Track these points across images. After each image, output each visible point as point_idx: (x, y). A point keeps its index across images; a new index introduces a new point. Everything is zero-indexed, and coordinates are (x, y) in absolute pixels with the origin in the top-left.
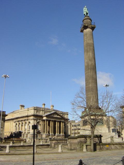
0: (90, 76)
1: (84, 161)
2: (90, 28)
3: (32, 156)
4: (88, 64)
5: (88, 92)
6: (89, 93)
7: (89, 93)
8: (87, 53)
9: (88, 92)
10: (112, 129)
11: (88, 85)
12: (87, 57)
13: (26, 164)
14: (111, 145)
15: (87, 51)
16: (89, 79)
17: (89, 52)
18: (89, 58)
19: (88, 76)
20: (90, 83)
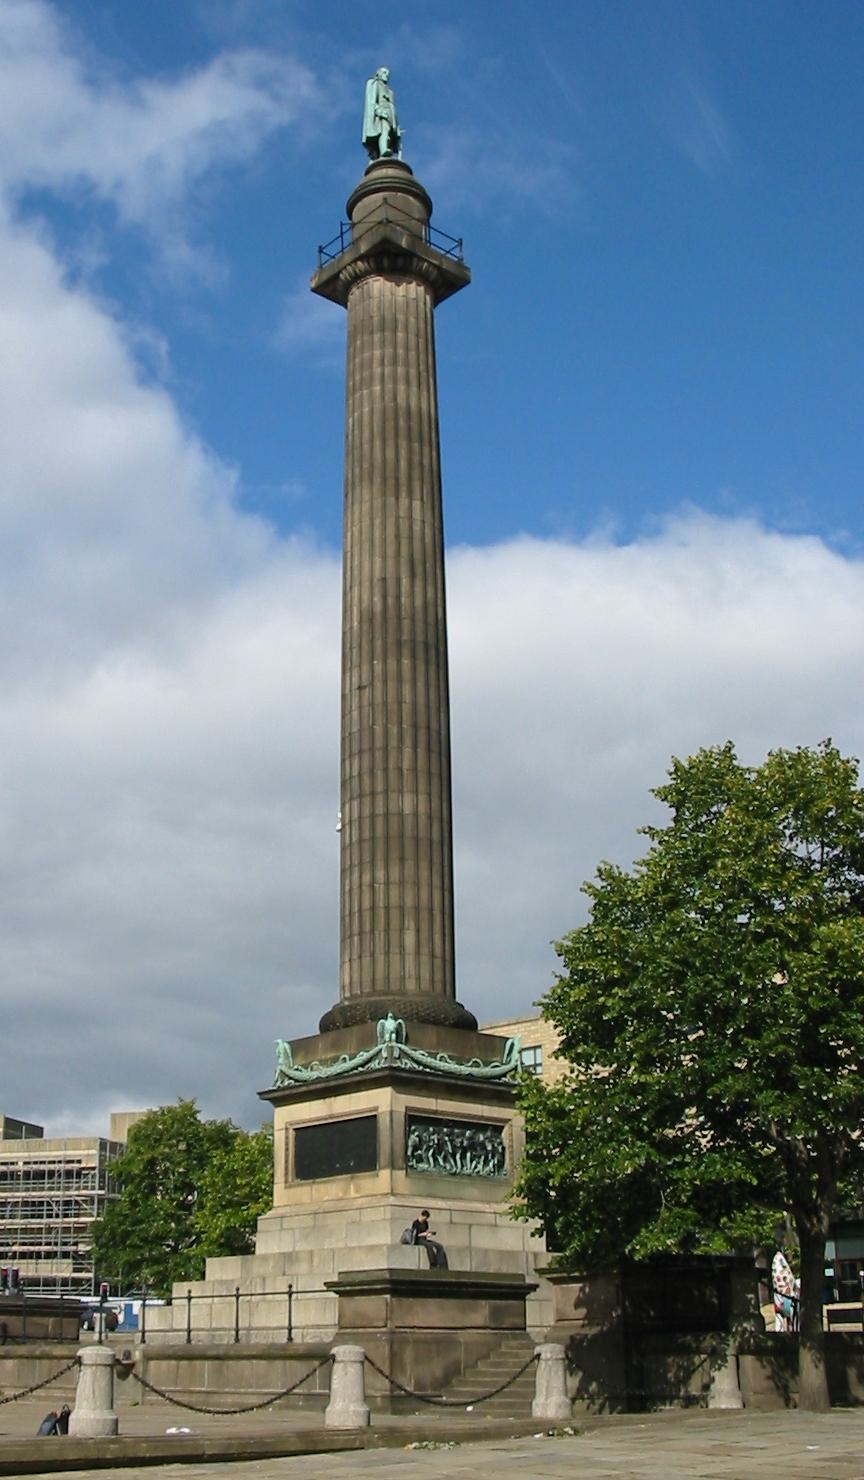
0: (406, 709)
4: (390, 601)
5: (380, 864)
7: (395, 875)
8: (391, 500)
9: (380, 864)
12: (391, 530)
14: (357, 278)
15: (391, 482)
16: (393, 742)
17: (403, 494)
18: (404, 542)
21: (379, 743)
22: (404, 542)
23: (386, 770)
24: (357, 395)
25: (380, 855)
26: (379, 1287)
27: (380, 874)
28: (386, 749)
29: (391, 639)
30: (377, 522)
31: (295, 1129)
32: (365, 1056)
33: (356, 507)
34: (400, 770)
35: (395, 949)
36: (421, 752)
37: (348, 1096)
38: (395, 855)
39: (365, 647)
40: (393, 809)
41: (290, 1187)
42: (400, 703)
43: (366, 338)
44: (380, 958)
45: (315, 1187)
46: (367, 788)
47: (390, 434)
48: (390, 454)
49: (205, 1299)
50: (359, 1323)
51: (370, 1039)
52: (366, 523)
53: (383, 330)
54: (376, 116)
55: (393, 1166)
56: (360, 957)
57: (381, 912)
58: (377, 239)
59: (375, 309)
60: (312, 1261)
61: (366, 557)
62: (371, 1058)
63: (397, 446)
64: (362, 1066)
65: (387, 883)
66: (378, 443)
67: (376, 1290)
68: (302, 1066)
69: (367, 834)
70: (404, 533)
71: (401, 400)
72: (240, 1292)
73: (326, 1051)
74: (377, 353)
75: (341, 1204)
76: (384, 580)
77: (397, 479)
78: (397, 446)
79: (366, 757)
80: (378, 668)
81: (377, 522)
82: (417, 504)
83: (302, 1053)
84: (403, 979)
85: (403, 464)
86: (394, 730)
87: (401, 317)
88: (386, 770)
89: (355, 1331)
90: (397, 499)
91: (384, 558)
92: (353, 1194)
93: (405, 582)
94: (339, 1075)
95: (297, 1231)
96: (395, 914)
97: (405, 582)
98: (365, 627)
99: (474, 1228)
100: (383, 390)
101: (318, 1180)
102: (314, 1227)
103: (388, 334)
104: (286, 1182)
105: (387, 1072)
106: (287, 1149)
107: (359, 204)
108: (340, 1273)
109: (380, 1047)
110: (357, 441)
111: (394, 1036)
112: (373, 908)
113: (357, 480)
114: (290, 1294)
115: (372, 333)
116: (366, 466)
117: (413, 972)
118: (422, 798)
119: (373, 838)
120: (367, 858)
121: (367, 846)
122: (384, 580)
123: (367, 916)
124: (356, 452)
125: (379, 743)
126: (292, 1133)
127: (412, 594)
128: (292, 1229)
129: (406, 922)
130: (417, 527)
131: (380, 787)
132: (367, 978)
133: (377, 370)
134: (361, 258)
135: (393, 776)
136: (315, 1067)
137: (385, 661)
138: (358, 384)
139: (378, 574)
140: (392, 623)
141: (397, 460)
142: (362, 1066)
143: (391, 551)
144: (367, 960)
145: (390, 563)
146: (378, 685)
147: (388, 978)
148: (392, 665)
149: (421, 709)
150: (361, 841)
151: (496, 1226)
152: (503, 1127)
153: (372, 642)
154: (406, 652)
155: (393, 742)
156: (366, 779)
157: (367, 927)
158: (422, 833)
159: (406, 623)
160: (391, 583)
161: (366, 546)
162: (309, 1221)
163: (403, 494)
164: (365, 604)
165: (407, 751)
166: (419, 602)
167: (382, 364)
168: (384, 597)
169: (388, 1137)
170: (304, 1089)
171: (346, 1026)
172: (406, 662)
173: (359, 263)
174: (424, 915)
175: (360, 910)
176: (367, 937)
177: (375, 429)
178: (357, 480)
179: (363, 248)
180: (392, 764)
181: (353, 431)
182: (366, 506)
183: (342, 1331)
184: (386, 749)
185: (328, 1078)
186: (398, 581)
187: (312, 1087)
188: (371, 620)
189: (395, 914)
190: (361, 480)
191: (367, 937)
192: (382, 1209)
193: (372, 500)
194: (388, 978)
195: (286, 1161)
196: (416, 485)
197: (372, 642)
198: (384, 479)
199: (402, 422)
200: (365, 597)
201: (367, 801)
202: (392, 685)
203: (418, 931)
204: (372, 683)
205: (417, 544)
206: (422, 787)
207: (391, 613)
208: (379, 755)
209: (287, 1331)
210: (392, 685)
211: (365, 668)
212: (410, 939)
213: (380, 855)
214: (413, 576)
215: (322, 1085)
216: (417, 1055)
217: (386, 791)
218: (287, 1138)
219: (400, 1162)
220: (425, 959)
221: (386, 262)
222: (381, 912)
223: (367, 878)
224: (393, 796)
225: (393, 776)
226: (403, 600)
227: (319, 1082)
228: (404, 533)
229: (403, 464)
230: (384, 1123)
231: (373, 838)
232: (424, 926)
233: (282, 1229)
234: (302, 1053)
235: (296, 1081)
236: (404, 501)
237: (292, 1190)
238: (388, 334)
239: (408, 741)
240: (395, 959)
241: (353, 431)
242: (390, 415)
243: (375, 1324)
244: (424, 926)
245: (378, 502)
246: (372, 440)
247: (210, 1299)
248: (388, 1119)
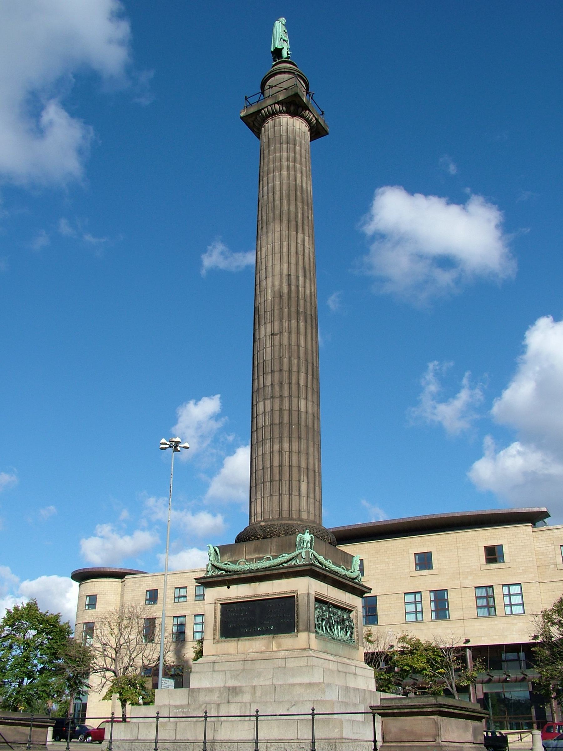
0: (302, 350)
1: (528, 530)
2: (308, 121)
3: (249, 714)
4: (293, 288)
5: (286, 440)
6: (290, 441)
7: (295, 447)
8: (293, 233)
9: (286, 440)
10: (366, 654)
11: (290, 396)
12: (293, 249)
13: (192, 732)
14: (274, 114)
15: (293, 223)
16: (295, 369)
17: (300, 231)
18: (301, 257)
19: (294, 347)
20: (302, 389)
21: (286, 368)
22: (301, 257)
23: (290, 383)
24: (271, 175)
25: (286, 434)
26: (429, 710)
27: (286, 446)
28: (290, 372)
29: (293, 309)
30: (285, 244)
31: (221, 604)
32: (288, 557)
33: (270, 234)
34: (299, 384)
35: (295, 492)
36: (310, 377)
37: (271, 582)
38: (295, 435)
39: (277, 312)
40: (294, 408)
41: (218, 642)
42: (298, 346)
43: (278, 146)
44: (286, 498)
45: (240, 643)
46: (277, 394)
47: (292, 198)
48: (293, 208)
49: (236, 718)
50: (404, 739)
51: (293, 546)
52: (277, 244)
53: (288, 143)
54: (281, 38)
55: (308, 630)
56: (271, 495)
57: (286, 469)
58: (291, 93)
59: (284, 132)
60: (255, 693)
61: (277, 262)
62: (293, 558)
63: (296, 205)
64: (285, 563)
65: (290, 452)
66: (285, 202)
67: (394, 713)
68: (230, 562)
69: (277, 421)
70: (301, 253)
71: (298, 181)
72: (208, 715)
73: (250, 553)
74: (285, 155)
75: (266, 655)
76: (289, 275)
77: (297, 222)
78: (296, 205)
79: (277, 375)
80: (285, 324)
81: (285, 244)
82: (306, 238)
83: (229, 554)
84: (300, 511)
85: (300, 215)
86: (295, 361)
87: (298, 139)
88: (290, 383)
89: (402, 744)
90: (297, 233)
91: (289, 263)
92: (274, 647)
93: (301, 279)
94: (266, 569)
95: (227, 673)
96: (295, 471)
97: (301, 279)
98: (277, 300)
99: (348, 674)
100: (288, 174)
101: (242, 638)
102: (244, 670)
103: (291, 146)
104: (214, 639)
105: (308, 567)
106: (215, 617)
107: (273, 78)
108: (381, 699)
109: (300, 551)
110: (271, 199)
111: (309, 545)
112: (281, 466)
113: (271, 220)
114: (313, 715)
115: (281, 143)
116: (277, 212)
117: (306, 508)
118: (310, 404)
119: (281, 423)
120: (277, 434)
121: (276, 428)
122: (289, 275)
123: (276, 471)
124: (270, 205)
125: (286, 368)
126: (219, 606)
127: (305, 287)
128: (225, 671)
129: (302, 477)
130: (307, 251)
131: (286, 393)
132: (276, 509)
133: (285, 163)
134: (278, 103)
135: (294, 387)
136: (241, 563)
137: (290, 321)
138: (272, 169)
139: (285, 272)
140: (294, 300)
141: (297, 212)
142: (285, 563)
143: (293, 260)
144: (276, 498)
145: (293, 267)
146: (286, 335)
147: (290, 510)
148: (294, 323)
149: (310, 352)
150: (272, 424)
151: (355, 674)
152: (352, 611)
153: (281, 309)
154: (302, 318)
155: (295, 369)
156: (277, 388)
157: (277, 478)
158: (310, 425)
159: (302, 302)
160: (293, 278)
161: (277, 256)
162: (239, 666)
163: (300, 231)
164: (277, 288)
165: (303, 375)
166: (308, 292)
167: (288, 160)
168: (289, 285)
169: (307, 611)
170: (236, 577)
171: (265, 538)
172: (302, 324)
173: (277, 106)
174: (311, 473)
175: (272, 467)
176: (276, 484)
177: (284, 194)
178: (271, 220)
179: (281, 98)
180: (294, 381)
181: (268, 193)
182: (277, 235)
183: (387, 744)
184: (290, 372)
185: (258, 570)
186: (297, 278)
187: (242, 576)
188: (281, 297)
189: (295, 471)
190: (274, 219)
191: (276, 484)
192: (305, 658)
193: (281, 231)
194: (290, 510)
195: (215, 625)
196: (306, 228)
197: (281, 309)
198: (289, 221)
199: (299, 194)
200: (277, 283)
201: (277, 401)
202: (294, 336)
203: (308, 483)
204: (281, 333)
205: (307, 259)
206: (310, 398)
207: (293, 295)
208: (285, 375)
209: (373, 743)
210: (294, 336)
211: (277, 324)
212: (304, 486)
213: (286, 434)
214: (305, 276)
215: (253, 574)
216: (321, 558)
217: (290, 396)
218: (215, 609)
219: (312, 628)
220: (311, 500)
221: (292, 108)
222: (286, 469)
223: (277, 447)
224: (295, 400)
225: (294, 387)
226: (300, 289)
227: (250, 572)
228: (301, 253)
229: (300, 215)
230: (302, 603)
231: (281, 423)
232: (311, 480)
233: (214, 671)
234: (229, 554)
235: (226, 571)
236: (300, 235)
237: (219, 645)
238: (291, 146)
239: (303, 369)
240: (295, 498)
241: (268, 193)
242: (292, 188)
243: (424, 739)
244: (311, 480)
245: (285, 233)
246: (281, 199)
247: (168, 719)
248: (306, 598)
